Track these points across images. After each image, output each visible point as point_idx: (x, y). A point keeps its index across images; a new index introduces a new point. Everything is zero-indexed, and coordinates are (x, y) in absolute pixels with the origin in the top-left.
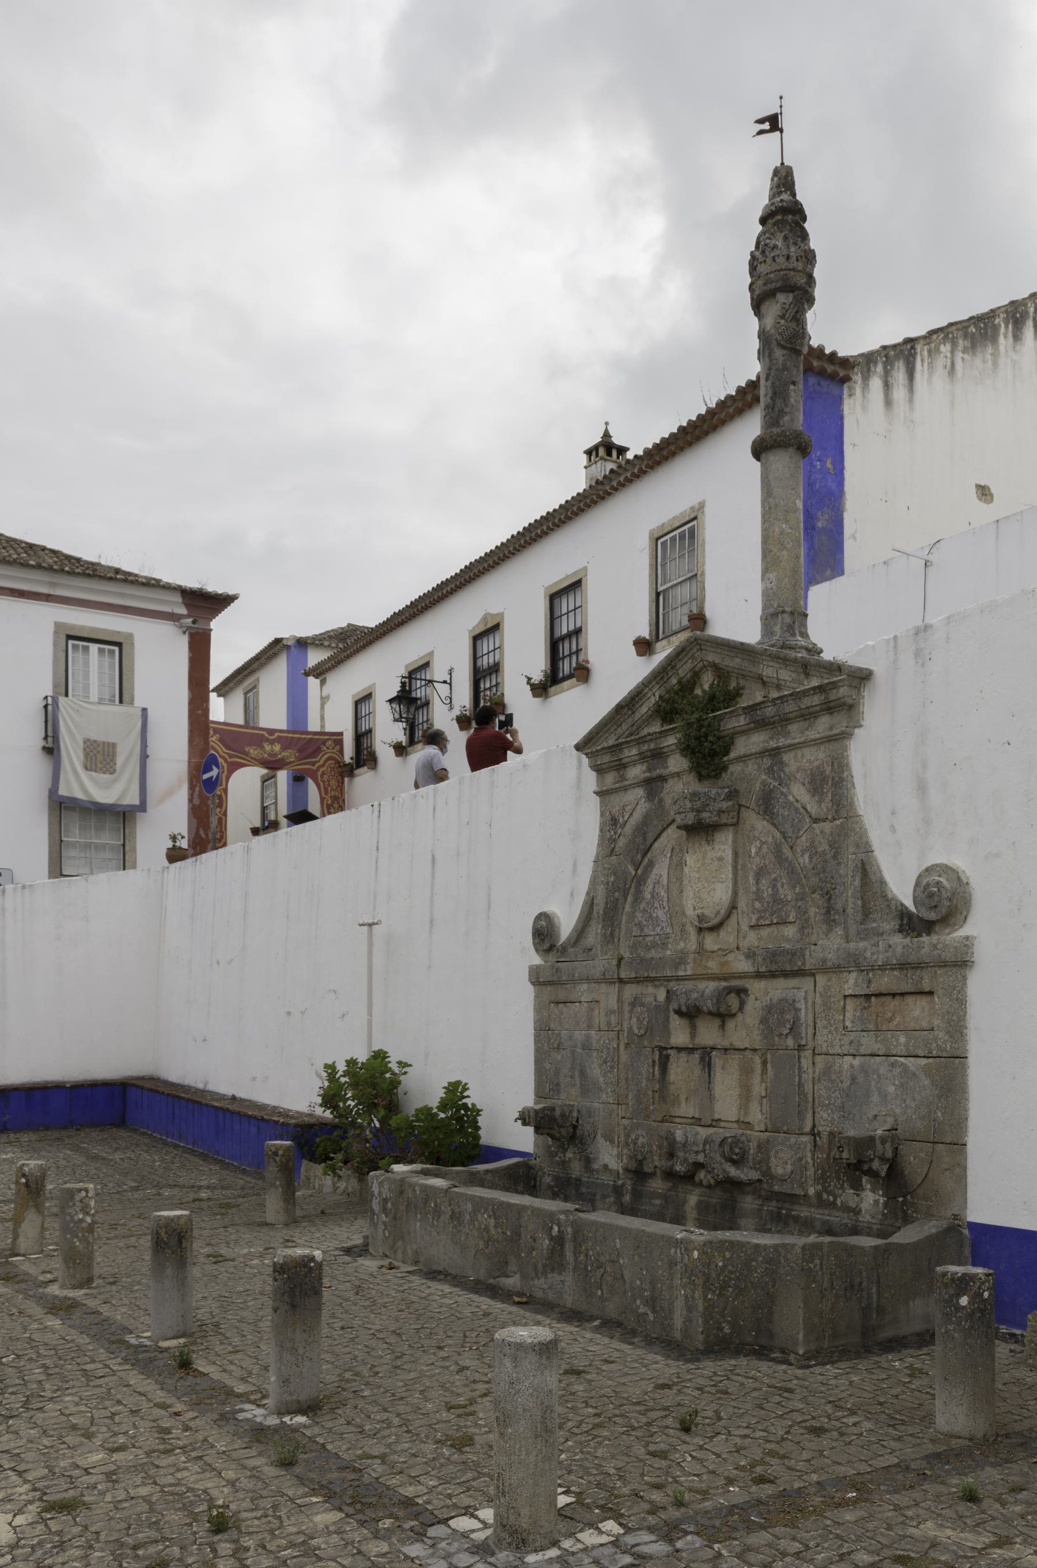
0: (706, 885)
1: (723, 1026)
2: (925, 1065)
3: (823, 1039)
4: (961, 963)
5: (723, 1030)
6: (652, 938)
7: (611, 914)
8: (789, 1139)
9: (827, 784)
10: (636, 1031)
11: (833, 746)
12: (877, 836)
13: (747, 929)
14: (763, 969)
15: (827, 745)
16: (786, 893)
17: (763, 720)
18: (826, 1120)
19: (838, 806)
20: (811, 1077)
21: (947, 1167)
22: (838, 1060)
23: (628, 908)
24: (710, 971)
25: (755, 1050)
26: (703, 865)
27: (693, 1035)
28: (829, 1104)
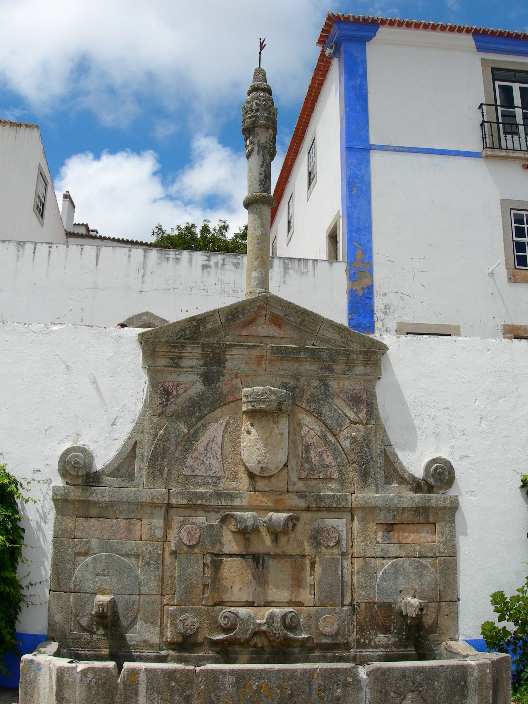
3: (358, 548)
8: (335, 610)
10: (186, 542)
13: (296, 480)
18: (361, 596)
20: (350, 571)
21: (445, 614)
28: (366, 586)
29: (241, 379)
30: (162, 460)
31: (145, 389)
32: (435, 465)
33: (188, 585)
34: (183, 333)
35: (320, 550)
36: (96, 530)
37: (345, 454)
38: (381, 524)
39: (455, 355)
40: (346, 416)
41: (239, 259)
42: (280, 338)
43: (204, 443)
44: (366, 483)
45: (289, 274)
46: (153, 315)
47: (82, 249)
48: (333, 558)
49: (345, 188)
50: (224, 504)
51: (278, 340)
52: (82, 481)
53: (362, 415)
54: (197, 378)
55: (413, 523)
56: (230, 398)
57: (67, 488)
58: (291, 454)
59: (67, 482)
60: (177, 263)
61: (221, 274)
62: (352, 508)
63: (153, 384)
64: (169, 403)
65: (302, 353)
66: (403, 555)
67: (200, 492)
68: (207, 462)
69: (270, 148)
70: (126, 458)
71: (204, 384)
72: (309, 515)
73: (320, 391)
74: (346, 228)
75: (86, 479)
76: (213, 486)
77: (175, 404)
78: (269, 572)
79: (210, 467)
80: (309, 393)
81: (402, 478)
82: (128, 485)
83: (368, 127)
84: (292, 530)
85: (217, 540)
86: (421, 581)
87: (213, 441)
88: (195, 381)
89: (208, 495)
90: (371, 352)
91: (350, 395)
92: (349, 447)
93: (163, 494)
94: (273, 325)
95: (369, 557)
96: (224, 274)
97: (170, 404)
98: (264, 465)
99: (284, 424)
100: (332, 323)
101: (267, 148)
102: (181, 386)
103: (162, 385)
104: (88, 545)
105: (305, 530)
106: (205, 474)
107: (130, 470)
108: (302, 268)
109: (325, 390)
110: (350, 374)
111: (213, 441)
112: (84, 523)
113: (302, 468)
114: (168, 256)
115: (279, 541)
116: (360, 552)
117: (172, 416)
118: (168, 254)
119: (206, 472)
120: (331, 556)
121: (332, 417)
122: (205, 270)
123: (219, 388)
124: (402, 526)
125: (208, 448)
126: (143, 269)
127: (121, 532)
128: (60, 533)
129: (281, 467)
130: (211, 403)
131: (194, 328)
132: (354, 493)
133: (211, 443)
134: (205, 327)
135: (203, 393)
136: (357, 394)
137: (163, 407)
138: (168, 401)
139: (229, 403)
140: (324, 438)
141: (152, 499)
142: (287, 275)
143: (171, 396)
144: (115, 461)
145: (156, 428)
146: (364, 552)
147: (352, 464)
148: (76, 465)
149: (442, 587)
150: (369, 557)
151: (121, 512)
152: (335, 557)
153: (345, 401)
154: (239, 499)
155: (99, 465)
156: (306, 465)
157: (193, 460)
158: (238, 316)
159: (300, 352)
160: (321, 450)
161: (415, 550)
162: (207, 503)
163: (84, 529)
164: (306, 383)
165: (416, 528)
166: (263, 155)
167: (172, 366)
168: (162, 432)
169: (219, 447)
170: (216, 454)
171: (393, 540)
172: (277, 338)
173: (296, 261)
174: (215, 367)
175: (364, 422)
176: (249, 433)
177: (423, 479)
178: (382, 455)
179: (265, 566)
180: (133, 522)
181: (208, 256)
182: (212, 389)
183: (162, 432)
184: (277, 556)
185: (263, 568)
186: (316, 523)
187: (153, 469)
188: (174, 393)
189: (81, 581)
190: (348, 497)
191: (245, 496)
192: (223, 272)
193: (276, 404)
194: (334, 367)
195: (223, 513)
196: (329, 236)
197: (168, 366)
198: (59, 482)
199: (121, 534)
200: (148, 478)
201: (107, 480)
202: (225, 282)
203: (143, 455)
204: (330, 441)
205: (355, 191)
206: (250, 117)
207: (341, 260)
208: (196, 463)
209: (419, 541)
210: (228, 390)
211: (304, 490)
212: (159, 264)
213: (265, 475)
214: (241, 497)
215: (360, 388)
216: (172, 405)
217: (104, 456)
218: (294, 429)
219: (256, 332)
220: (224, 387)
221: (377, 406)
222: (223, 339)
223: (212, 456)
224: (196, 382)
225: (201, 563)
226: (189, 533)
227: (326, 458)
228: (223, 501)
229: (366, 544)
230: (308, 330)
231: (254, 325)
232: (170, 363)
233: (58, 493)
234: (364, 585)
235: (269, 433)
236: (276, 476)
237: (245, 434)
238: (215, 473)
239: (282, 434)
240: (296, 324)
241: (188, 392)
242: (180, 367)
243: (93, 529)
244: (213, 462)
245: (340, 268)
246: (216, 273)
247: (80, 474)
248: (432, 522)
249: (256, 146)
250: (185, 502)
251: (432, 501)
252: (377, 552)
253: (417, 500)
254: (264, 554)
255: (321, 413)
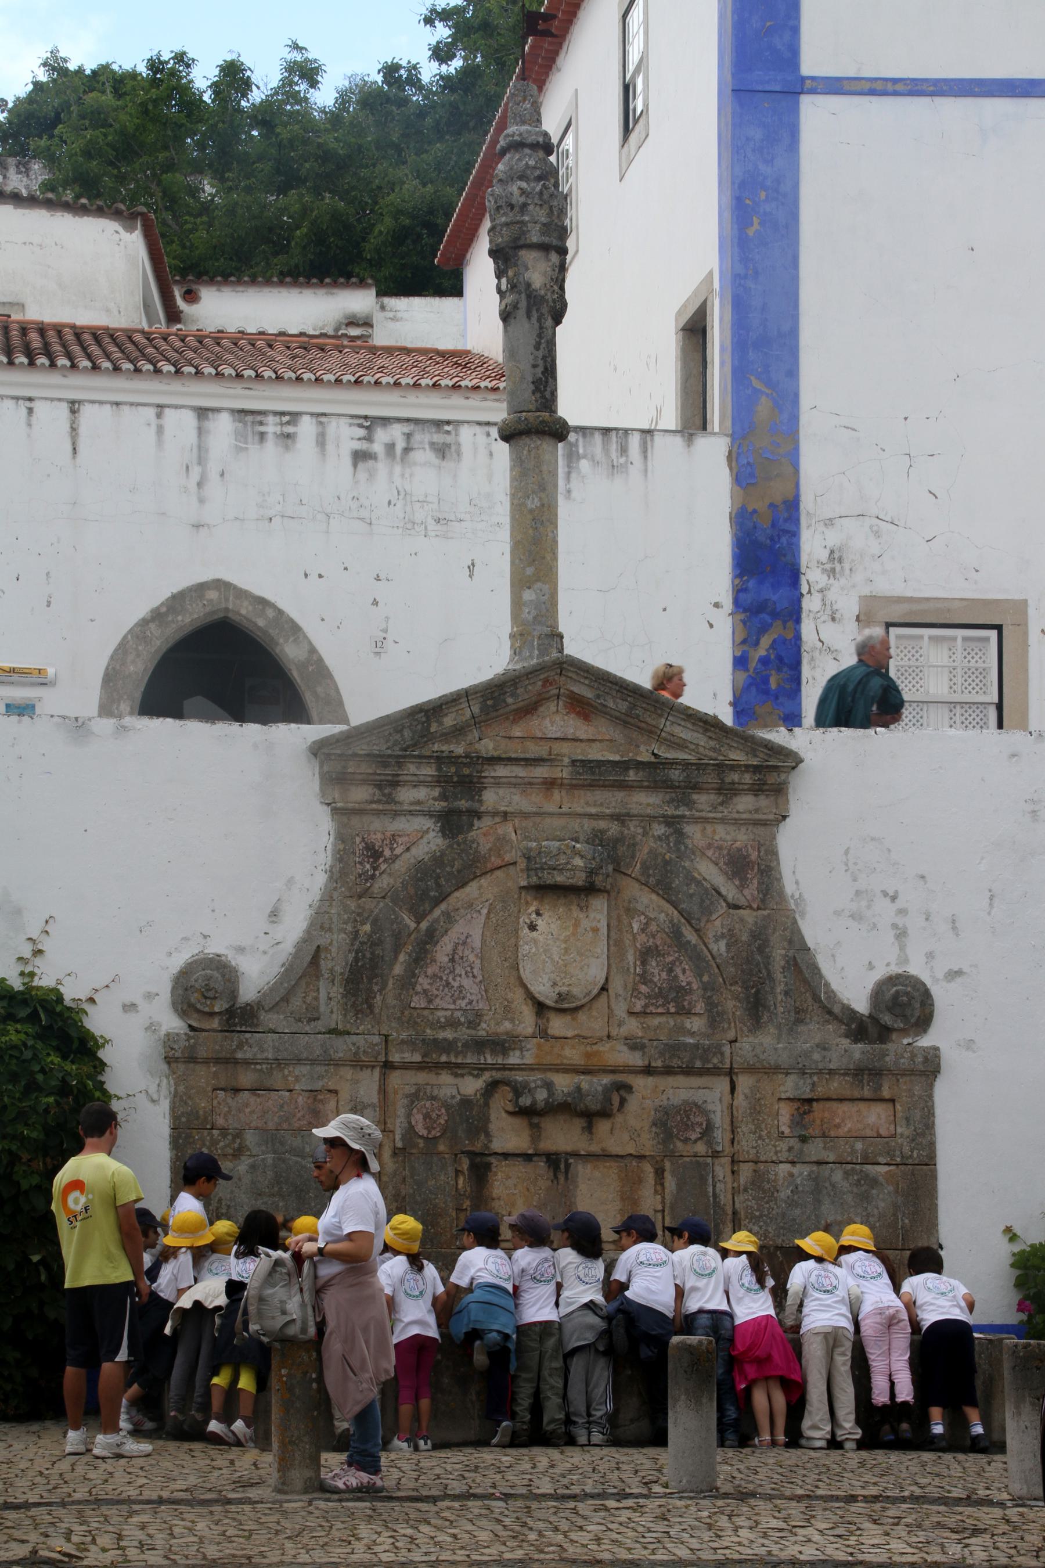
0: (578, 958)
1: (589, 1128)
2: (886, 1173)
4: (930, 1067)
5: (591, 1133)
6: (449, 1013)
7: (362, 978)
9: (752, 870)
11: (761, 831)
12: (815, 931)
13: (624, 1015)
14: (659, 1063)
15: (750, 828)
16: (686, 977)
17: (665, 781)
19: (765, 895)
22: (772, 1166)
23: (398, 969)
24: (565, 1061)
25: (641, 1157)
26: (573, 934)
27: (535, 1138)
28: (761, 1216)
29: (514, 825)
30: (370, 980)
31: (329, 847)
32: (895, 989)
33: (428, 1210)
34: (398, 737)
35: (672, 1147)
36: (252, 1112)
37: (718, 967)
38: (788, 1099)
39: (940, 767)
40: (719, 893)
41: (448, 432)
42: (589, 740)
43: (449, 948)
44: (758, 1022)
45: (579, 472)
46: (235, 587)
47: (30, 411)
48: (698, 1162)
49: (727, 214)
50: (489, 1061)
51: (583, 745)
52: (220, 1024)
53: (752, 890)
54: (428, 823)
55: (850, 1100)
56: (495, 861)
57: (193, 1038)
58: (614, 966)
59: (190, 1026)
60: (287, 448)
61: (403, 475)
62: (731, 1068)
63: (342, 838)
64: (377, 873)
65: (631, 773)
66: (831, 1159)
67: (445, 1039)
68: (456, 984)
69: (554, 301)
70: (300, 978)
71: (444, 836)
72: (650, 1081)
73: (668, 845)
74: (728, 334)
75: (228, 1020)
76: (468, 1028)
77: (390, 874)
78: (577, 1187)
79: (461, 992)
80: (646, 850)
81: (830, 1012)
82: (307, 1029)
83: (798, 18)
84: (619, 1110)
85: (480, 1127)
86: (866, 1208)
87: (464, 943)
88: (425, 828)
89: (460, 1045)
90: (767, 766)
91: (725, 852)
92: (725, 954)
93: (376, 1045)
94: (573, 716)
95: (766, 1162)
96: (411, 475)
97: (380, 874)
98: (564, 989)
99: (599, 911)
100: (691, 712)
101: (547, 301)
102: (400, 840)
103: (363, 838)
104: (238, 1141)
105: (643, 1109)
106: (452, 1007)
107: (309, 999)
108: (614, 455)
109: (678, 843)
110: (726, 811)
111: (464, 943)
112: (229, 1100)
113: (635, 993)
114: (262, 429)
115: (594, 1130)
116: (748, 1152)
117: (384, 897)
118: (261, 423)
119: (454, 1003)
120: (694, 1159)
121: (691, 896)
122: (360, 465)
123: (473, 841)
124: (828, 1104)
125: (457, 957)
126: (199, 463)
127: (299, 1115)
128: (184, 1119)
129: (595, 992)
130: (459, 871)
131: (419, 727)
132: (736, 1041)
133: (461, 948)
134: (441, 724)
135: (443, 853)
136: (739, 850)
137: (366, 880)
138: (375, 869)
139: (492, 870)
140: (676, 934)
141: (356, 1054)
142: (573, 475)
143: (381, 860)
144: (282, 984)
145: (356, 921)
146: (755, 1151)
147: (731, 985)
148: (208, 993)
149: (907, 1221)
150: (766, 1162)
151: (297, 1079)
152: (701, 1159)
153: (717, 864)
154: (517, 1053)
155: (248, 992)
156: (643, 989)
157: (429, 981)
158: (505, 701)
159: (627, 769)
160: (671, 958)
161: (853, 1151)
162: (460, 1061)
163: (229, 1112)
164: (640, 831)
165: (855, 1109)
166: (539, 320)
167: (378, 802)
168: (367, 928)
169: (477, 956)
170: (472, 968)
171: (811, 1131)
172: (581, 741)
173: (598, 437)
174: (463, 802)
175: (755, 906)
176: (533, 927)
177: (870, 1016)
178: (789, 969)
179: (570, 1176)
180: (320, 1097)
181: (367, 428)
182: (459, 844)
183: (367, 928)
184: (591, 1157)
185: (567, 1178)
186: (664, 1097)
187: (353, 999)
188: (387, 853)
189: (229, 1207)
190: (724, 1049)
191: (528, 1046)
192: (408, 471)
193: (583, 875)
194: (695, 797)
195: (487, 1076)
196: (684, 329)
197: (372, 802)
198: (172, 1023)
199: (299, 1119)
200: (345, 1015)
201: (270, 1019)
202: (415, 499)
203: (332, 970)
204: (689, 942)
205: (756, 225)
206: (507, 224)
207: (717, 429)
208: (435, 986)
209: (863, 1134)
210: (490, 845)
211: (640, 1034)
212: (239, 450)
213: (566, 1006)
214: (521, 1050)
215: (745, 837)
216: (384, 876)
217: (257, 974)
218: (619, 920)
219: (541, 730)
220: (482, 840)
221: (780, 873)
222: (477, 746)
223: (463, 973)
224: (427, 831)
225: (451, 1170)
226: (427, 1116)
227: (681, 975)
228: (488, 1056)
229: (760, 1137)
230: (643, 725)
231: (535, 717)
232: (374, 794)
233: (176, 1047)
234: (757, 1214)
235: (571, 929)
236: (586, 1009)
237: (526, 930)
238: (471, 1002)
239: (595, 930)
240: (618, 714)
241: (414, 851)
242: (396, 803)
243: (248, 1110)
244: (467, 983)
245: (713, 450)
246: (391, 473)
247: (217, 1010)
248: (887, 1097)
249: (523, 296)
250: (417, 1058)
251: (887, 1059)
252: (781, 1151)
253: (857, 1055)
254: (567, 1154)
255: (671, 888)
